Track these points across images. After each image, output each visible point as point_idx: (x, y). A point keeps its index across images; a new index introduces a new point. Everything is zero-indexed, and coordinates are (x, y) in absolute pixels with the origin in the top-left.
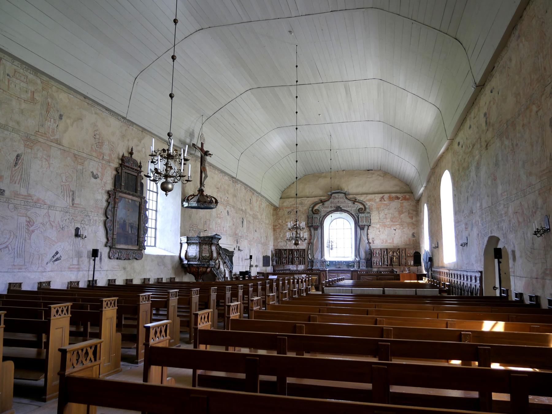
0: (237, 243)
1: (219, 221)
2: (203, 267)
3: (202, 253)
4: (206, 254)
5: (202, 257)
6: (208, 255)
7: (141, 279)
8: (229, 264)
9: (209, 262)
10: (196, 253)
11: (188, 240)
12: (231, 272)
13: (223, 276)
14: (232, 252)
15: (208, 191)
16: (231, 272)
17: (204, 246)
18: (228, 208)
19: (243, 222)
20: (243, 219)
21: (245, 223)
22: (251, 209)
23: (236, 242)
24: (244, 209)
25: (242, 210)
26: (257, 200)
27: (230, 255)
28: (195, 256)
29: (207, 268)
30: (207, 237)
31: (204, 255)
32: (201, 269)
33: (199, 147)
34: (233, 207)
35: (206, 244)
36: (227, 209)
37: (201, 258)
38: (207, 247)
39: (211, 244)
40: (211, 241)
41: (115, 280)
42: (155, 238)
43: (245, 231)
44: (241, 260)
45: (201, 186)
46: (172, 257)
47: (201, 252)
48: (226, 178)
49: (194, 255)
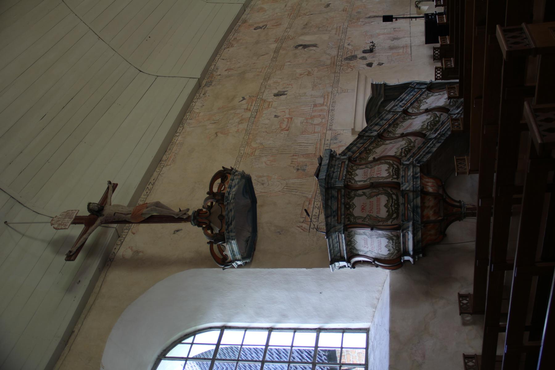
0: (354, 57)
1: (298, 121)
2: (423, 207)
3: (377, 219)
4: (380, 206)
5: (390, 216)
6: (383, 199)
7: (465, 324)
8: (407, 97)
9: (404, 194)
10: (379, 236)
11: (342, 259)
12: (431, 88)
13: (444, 117)
14: (375, 87)
15: (197, 200)
16: (431, 88)
17: (357, 212)
18: (268, 95)
19: (305, 46)
20: (297, 47)
21: (307, 39)
22: (278, 25)
23: (352, 63)
24: (274, 46)
25: (277, 51)
26: (261, 9)
27: (385, 100)
28: (390, 238)
29: (423, 193)
30: (326, 206)
31: (383, 213)
32: (430, 213)
33: (84, 232)
34: (267, 78)
35: (349, 207)
36: (271, 98)
37: (392, 226)
38: (358, 202)
39: (349, 189)
40: (339, 190)
41: (467, 357)
42: (344, 331)
43: (326, 37)
44: (396, 43)
45: (187, 220)
46: (397, 298)
47: (373, 224)
48: (197, 105)
49: (384, 241)
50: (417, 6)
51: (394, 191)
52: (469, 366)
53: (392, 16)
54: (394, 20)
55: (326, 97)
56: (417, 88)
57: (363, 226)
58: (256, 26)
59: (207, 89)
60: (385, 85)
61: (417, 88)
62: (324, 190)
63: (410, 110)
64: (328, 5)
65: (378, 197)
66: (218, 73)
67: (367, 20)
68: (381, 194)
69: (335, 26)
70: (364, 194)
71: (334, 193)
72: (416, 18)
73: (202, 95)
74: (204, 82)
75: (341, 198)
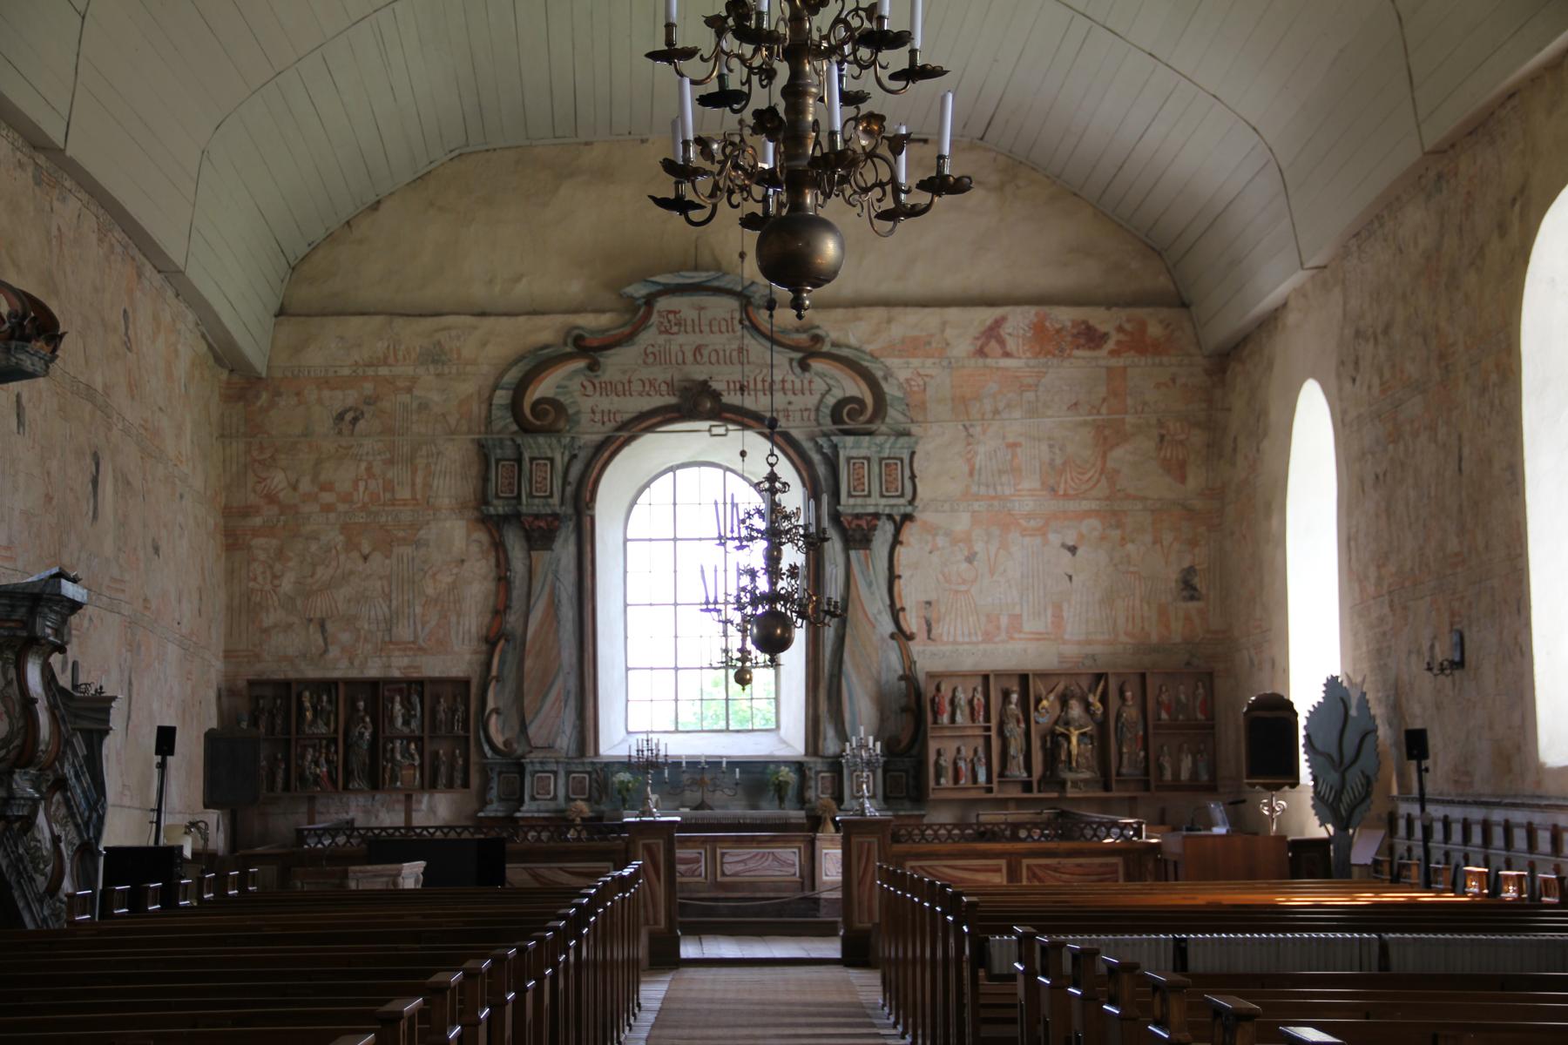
19: (95, 482)
40: (27, 624)
50: (193, 824)
51: (12, 755)
52: (1195, 773)
53: (172, 753)
54: (159, 759)
55: (8, 554)
56: (90, 817)
57: (1348, 857)
58: (130, 311)
59: (30, 169)
60: (106, 732)
61: (90, 817)
62: (36, 590)
63: (58, 796)
64: (156, 550)
65: (5, 717)
66: (56, 204)
67: (126, 674)
68: (11, 724)
69: (127, 577)
70: (9, 683)
71: (21, 612)
72: (158, 823)
73: (19, 154)
74: (41, 159)
75: (10, 628)
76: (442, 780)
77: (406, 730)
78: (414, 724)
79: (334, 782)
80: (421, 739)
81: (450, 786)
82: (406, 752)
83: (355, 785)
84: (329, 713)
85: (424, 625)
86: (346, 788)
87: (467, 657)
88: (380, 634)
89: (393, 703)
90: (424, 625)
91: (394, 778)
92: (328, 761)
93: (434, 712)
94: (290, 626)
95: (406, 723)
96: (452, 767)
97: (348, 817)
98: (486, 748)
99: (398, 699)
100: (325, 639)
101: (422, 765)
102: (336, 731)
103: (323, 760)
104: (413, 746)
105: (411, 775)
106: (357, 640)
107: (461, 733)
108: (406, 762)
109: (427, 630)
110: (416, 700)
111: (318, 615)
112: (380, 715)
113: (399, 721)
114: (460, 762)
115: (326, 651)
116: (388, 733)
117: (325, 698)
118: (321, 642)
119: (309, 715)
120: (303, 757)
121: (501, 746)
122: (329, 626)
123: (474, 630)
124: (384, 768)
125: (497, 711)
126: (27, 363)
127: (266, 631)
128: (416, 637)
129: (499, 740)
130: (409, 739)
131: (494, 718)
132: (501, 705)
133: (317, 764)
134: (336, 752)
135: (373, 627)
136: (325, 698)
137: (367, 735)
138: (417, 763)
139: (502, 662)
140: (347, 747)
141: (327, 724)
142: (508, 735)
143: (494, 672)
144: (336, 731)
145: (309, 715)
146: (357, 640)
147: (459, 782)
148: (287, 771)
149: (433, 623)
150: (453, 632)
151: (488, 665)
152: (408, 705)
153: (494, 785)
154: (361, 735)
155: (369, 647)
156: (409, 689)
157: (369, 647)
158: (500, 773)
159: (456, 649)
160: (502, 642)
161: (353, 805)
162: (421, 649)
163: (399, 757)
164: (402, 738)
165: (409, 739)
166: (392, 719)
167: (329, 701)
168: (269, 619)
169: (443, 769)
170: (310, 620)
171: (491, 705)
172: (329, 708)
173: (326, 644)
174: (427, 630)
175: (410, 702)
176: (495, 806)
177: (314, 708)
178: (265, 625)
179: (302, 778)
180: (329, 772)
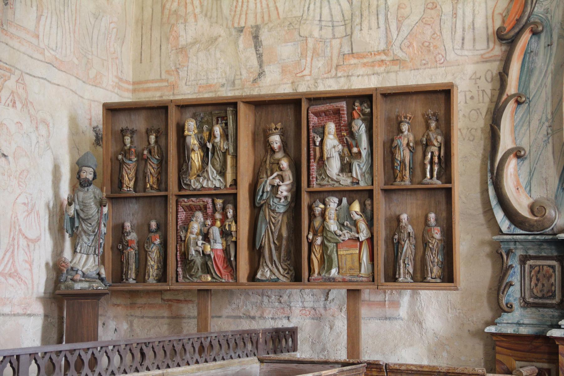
76: (406, 268)
77: (345, 181)
78: (359, 169)
79: (231, 266)
80: (370, 193)
81: (420, 276)
82: (346, 220)
83: (265, 273)
84: (225, 154)
85: (400, 23)
86: (252, 277)
87: (470, 69)
88: (336, 43)
89: (323, 135)
90: (400, 23)
91: (326, 262)
92: (225, 234)
93: (391, 150)
94: (213, 40)
95: (346, 168)
96: (424, 243)
97: (291, 325)
98: (499, 215)
99: (331, 127)
100: (260, 56)
101: (371, 240)
102: (235, 183)
103: (215, 231)
104: (356, 207)
105: (352, 259)
106: (303, 55)
107: (438, 183)
108: (347, 235)
109: (405, 31)
110: (360, 127)
111: (251, 22)
112: (302, 155)
113: (334, 167)
114: (437, 234)
115: (261, 74)
116: (315, 187)
117: (217, 130)
118: (254, 61)
119: (196, 158)
120: (186, 227)
121: (525, 213)
122: (265, 36)
123: (480, 22)
124: (311, 244)
125: (518, 154)
126: (487, 116)
127: (182, 50)
128: (389, 43)
129: (521, 203)
130: (351, 194)
131: (512, 165)
132: (524, 143)
133: (206, 237)
134: (235, 217)
135: (327, 33)
136: (217, 130)
137: (284, 190)
138: (363, 235)
139: (527, 71)
140: (256, 209)
141: (222, 173)
142: (538, 193)
143: (512, 88)
144: (235, 183)
145: (196, 158)
146: (303, 55)
147: (436, 271)
148: (164, 245)
149: (415, 18)
150: (447, 35)
151: (502, 77)
152: (347, 136)
153: (515, 277)
154: (275, 188)
155: (320, 63)
156: (351, 109)
157: (320, 63)
158: (524, 260)
159: (451, 56)
160: (526, 36)
161: (297, 305)
162: (396, 61)
163: (333, 226)
164: (340, 193)
165: (351, 194)
166: (322, 162)
167: (225, 135)
168: (188, 33)
169: (407, 248)
170: (241, 30)
171: (506, 142)
172: (223, 145)
173: (261, 66)
174: (405, 31)
175: (352, 134)
176: (518, 314)
177: (203, 147)
178: (182, 42)
179: (185, 259)
180: (226, 251)
